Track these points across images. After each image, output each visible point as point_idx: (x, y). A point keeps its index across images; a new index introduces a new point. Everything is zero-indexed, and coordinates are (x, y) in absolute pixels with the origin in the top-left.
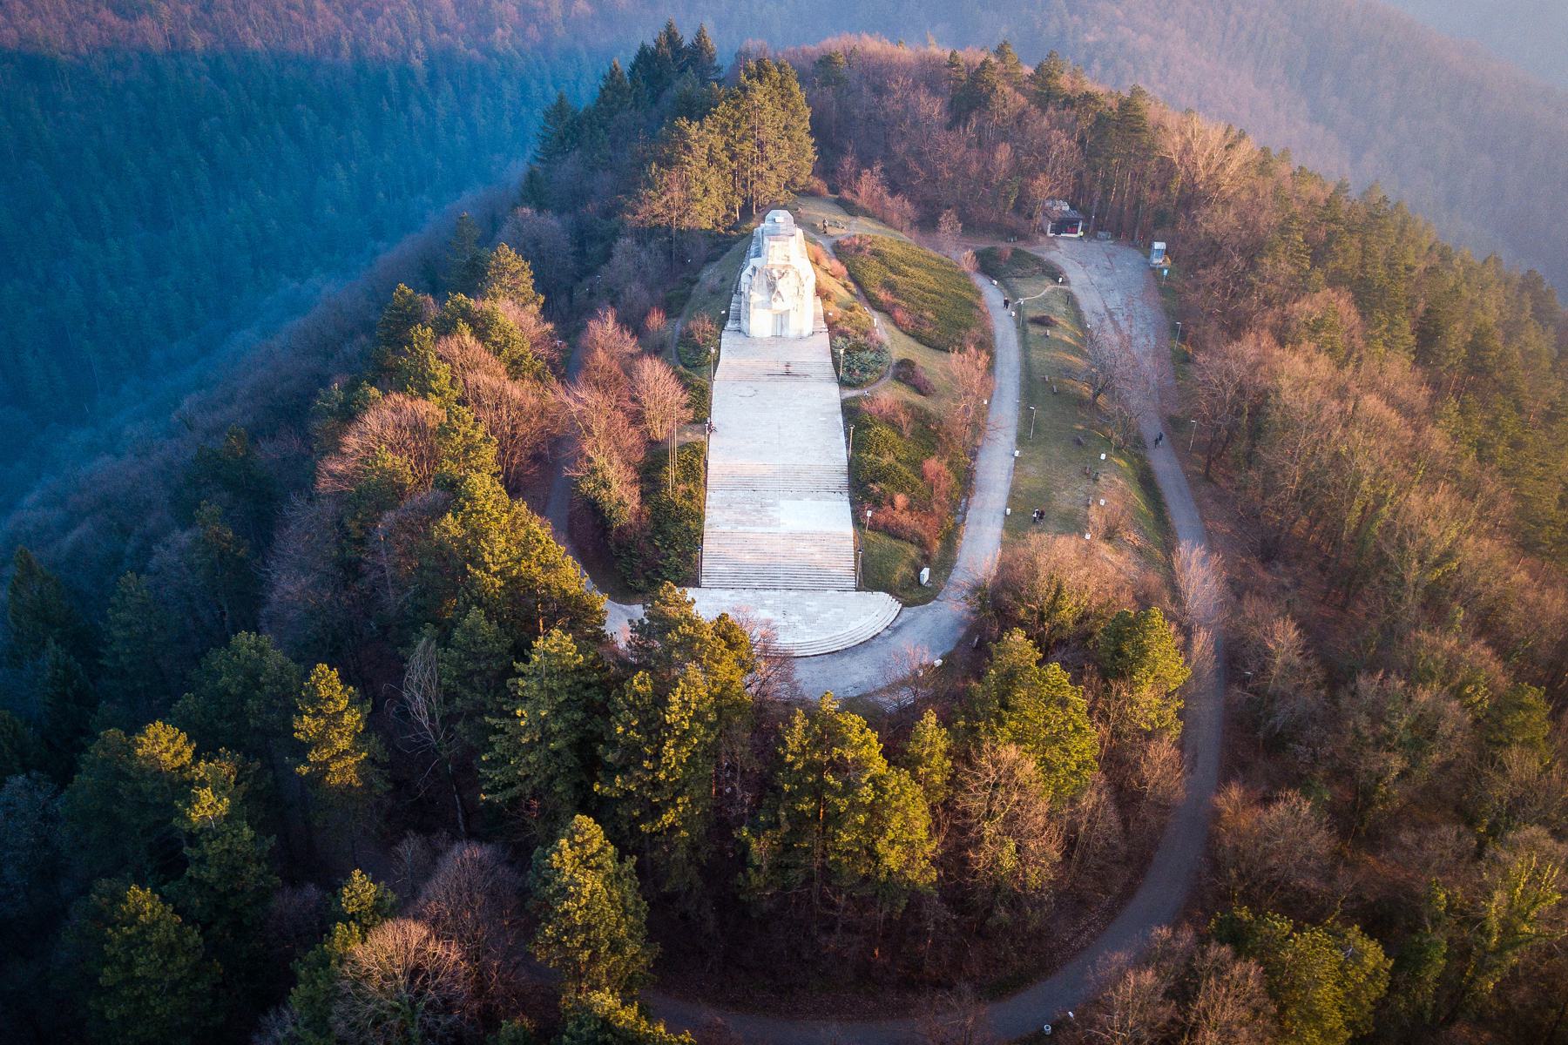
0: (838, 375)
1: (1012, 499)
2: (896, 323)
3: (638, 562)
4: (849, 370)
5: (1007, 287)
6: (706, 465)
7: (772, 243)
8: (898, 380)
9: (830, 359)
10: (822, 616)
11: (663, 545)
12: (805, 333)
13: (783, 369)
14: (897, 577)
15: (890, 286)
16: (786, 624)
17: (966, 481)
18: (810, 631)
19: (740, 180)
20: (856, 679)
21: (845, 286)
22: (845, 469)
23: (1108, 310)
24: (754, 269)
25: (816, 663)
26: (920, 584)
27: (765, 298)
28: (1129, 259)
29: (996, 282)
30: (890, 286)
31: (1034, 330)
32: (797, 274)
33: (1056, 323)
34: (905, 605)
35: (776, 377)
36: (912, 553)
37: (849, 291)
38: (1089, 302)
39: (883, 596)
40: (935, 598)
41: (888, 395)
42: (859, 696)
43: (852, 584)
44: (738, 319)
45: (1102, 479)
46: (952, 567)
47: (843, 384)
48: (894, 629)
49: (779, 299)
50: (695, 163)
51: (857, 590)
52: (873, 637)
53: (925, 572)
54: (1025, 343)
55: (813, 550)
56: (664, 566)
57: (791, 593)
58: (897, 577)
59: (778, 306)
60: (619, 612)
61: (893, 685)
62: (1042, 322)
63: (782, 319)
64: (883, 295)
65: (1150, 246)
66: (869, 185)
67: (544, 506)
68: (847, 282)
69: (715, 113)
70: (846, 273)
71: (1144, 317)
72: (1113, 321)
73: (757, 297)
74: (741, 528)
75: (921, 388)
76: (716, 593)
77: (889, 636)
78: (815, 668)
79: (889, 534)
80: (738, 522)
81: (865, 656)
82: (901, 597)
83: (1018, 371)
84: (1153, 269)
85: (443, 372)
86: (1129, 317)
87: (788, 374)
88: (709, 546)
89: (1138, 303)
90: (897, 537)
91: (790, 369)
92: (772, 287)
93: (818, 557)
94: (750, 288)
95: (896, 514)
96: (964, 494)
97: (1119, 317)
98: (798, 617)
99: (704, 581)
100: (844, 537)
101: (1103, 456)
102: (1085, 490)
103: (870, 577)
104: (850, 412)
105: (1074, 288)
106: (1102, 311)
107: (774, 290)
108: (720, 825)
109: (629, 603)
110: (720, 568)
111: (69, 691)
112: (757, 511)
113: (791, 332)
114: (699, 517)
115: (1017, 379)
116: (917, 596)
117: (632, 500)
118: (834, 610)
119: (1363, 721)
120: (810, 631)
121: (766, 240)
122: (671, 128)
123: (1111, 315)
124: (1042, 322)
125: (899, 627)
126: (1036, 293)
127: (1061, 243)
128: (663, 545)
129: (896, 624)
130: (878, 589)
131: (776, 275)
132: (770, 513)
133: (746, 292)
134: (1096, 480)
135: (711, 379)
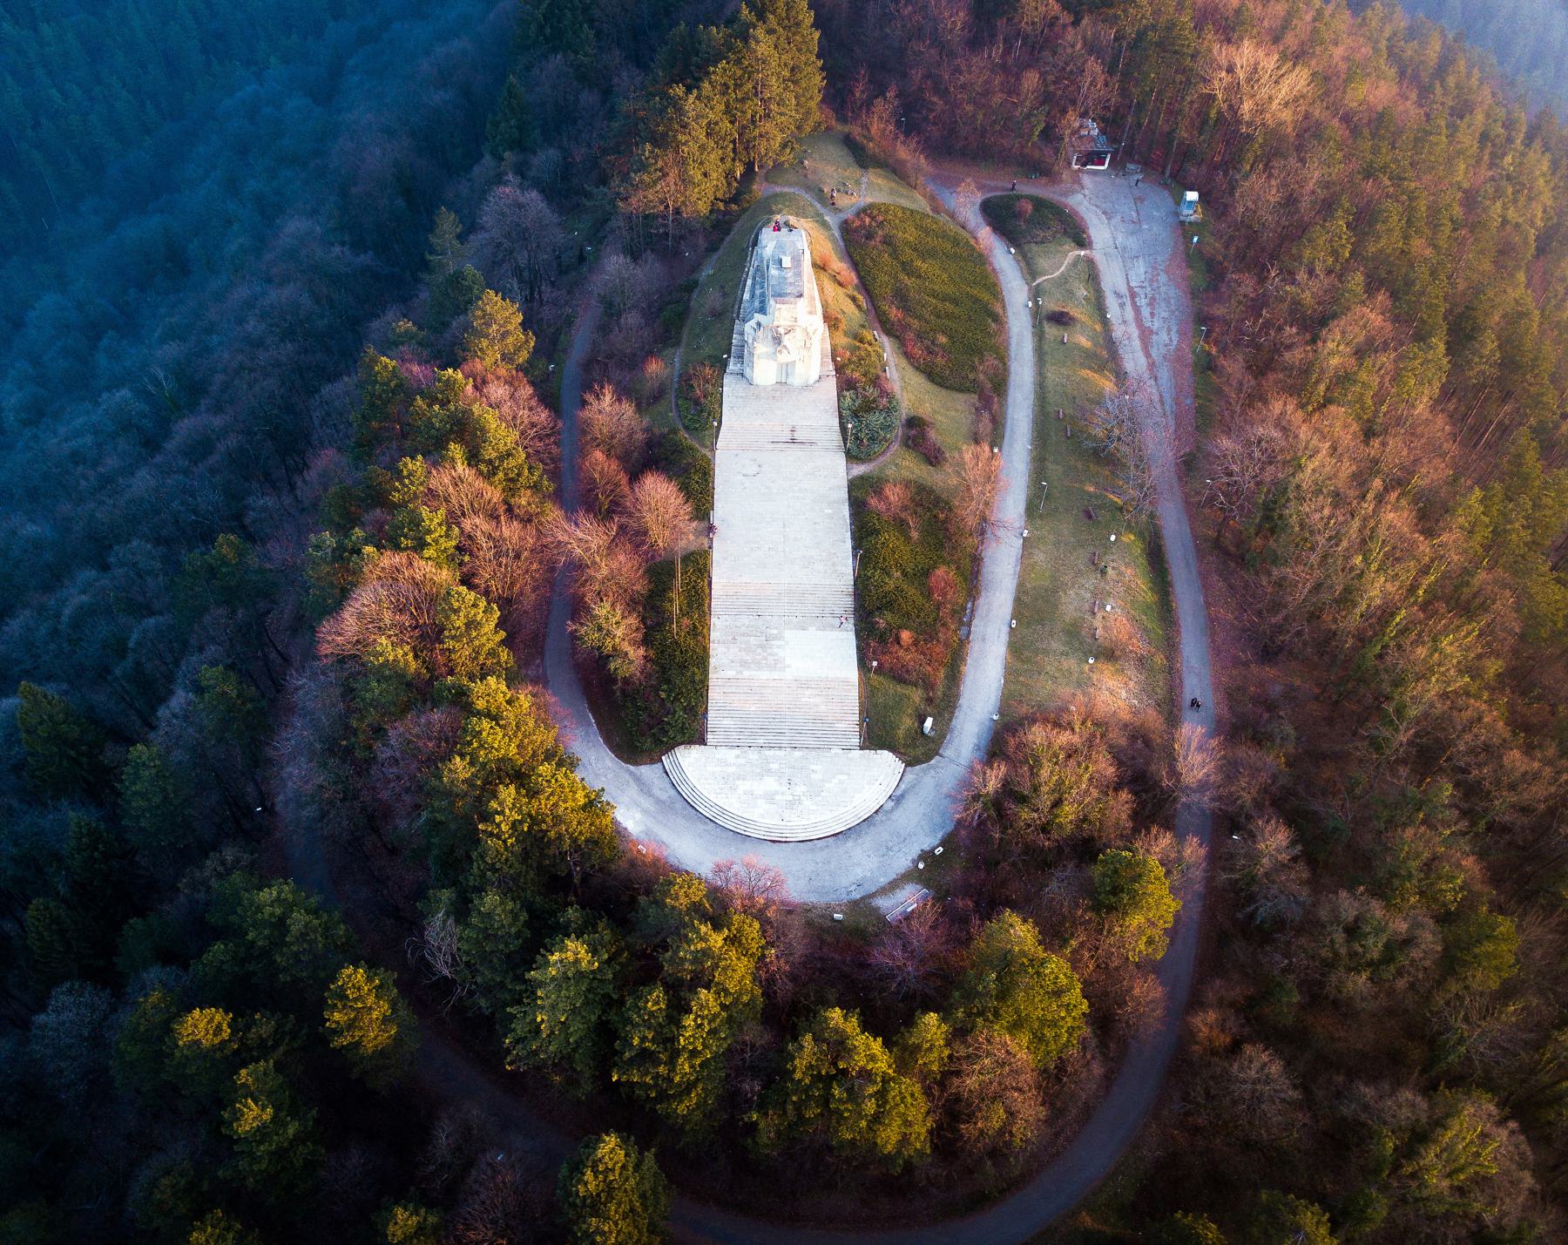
0: (845, 444)
1: (1018, 601)
2: (908, 355)
3: (643, 716)
4: (857, 438)
5: (1024, 257)
6: (710, 584)
7: (778, 306)
8: (908, 446)
9: (837, 420)
10: (827, 785)
11: (669, 696)
12: (811, 381)
13: (787, 436)
14: (901, 733)
15: (901, 297)
16: (791, 798)
17: (972, 577)
18: (814, 807)
19: (743, 145)
20: (859, 873)
21: (854, 299)
22: (851, 589)
23: (1130, 289)
24: (759, 324)
25: (822, 849)
26: (922, 732)
27: (771, 349)
28: (1157, 203)
29: (1013, 251)
30: (901, 297)
31: (1051, 331)
32: (805, 330)
33: (1072, 319)
34: (909, 764)
35: (780, 445)
36: (917, 700)
37: (859, 307)
38: (1112, 278)
39: (886, 755)
40: (937, 754)
41: (899, 465)
42: (862, 898)
43: (856, 741)
44: (741, 357)
45: (1109, 570)
46: (955, 708)
47: (851, 457)
48: (897, 799)
49: (785, 351)
50: (693, 140)
51: (862, 748)
52: (876, 812)
53: (929, 722)
54: (1039, 336)
55: (817, 700)
56: (669, 723)
57: (797, 753)
58: (901, 733)
59: (784, 358)
60: (627, 776)
61: (895, 881)
62: (1060, 319)
63: (787, 368)
64: (894, 313)
65: (1182, 196)
66: (878, 125)
67: (546, 616)
68: (856, 293)
69: (714, 72)
70: (856, 281)
71: (1167, 300)
72: (1134, 304)
73: (761, 349)
74: (746, 673)
75: (933, 457)
76: (723, 753)
77: (892, 810)
78: (820, 856)
79: (894, 677)
80: (744, 664)
81: (868, 840)
82: (904, 754)
83: (1032, 397)
84: (1182, 223)
85: (433, 519)
86: (1152, 302)
87: (793, 441)
88: (715, 695)
89: (1163, 278)
90: (901, 680)
91: (796, 435)
92: (777, 340)
93: (823, 708)
94: (754, 340)
95: (901, 653)
96: (970, 596)
97: (1142, 302)
98: (804, 789)
99: (709, 736)
100: (846, 682)
101: (1113, 538)
102: (1092, 588)
103: (876, 734)
104: (861, 496)
105: (1097, 256)
106: (1123, 290)
107: (779, 344)
108: (732, 1101)
109: (636, 763)
110: (726, 722)
111: (96, 854)
112: (761, 646)
113: (796, 380)
114: (702, 661)
115: (1030, 411)
116: (920, 751)
117: (636, 654)
118: (838, 777)
119: (1339, 937)
120: (814, 807)
121: (772, 302)
122: (665, 96)
123: (1133, 295)
124: (1060, 319)
125: (902, 796)
126: (1060, 261)
127: (1087, 180)
128: (669, 696)
129: (899, 793)
130: (882, 748)
131: (781, 330)
132: (775, 650)
133: (750, 341)
134: (1103, 572)
135: (713, 450)
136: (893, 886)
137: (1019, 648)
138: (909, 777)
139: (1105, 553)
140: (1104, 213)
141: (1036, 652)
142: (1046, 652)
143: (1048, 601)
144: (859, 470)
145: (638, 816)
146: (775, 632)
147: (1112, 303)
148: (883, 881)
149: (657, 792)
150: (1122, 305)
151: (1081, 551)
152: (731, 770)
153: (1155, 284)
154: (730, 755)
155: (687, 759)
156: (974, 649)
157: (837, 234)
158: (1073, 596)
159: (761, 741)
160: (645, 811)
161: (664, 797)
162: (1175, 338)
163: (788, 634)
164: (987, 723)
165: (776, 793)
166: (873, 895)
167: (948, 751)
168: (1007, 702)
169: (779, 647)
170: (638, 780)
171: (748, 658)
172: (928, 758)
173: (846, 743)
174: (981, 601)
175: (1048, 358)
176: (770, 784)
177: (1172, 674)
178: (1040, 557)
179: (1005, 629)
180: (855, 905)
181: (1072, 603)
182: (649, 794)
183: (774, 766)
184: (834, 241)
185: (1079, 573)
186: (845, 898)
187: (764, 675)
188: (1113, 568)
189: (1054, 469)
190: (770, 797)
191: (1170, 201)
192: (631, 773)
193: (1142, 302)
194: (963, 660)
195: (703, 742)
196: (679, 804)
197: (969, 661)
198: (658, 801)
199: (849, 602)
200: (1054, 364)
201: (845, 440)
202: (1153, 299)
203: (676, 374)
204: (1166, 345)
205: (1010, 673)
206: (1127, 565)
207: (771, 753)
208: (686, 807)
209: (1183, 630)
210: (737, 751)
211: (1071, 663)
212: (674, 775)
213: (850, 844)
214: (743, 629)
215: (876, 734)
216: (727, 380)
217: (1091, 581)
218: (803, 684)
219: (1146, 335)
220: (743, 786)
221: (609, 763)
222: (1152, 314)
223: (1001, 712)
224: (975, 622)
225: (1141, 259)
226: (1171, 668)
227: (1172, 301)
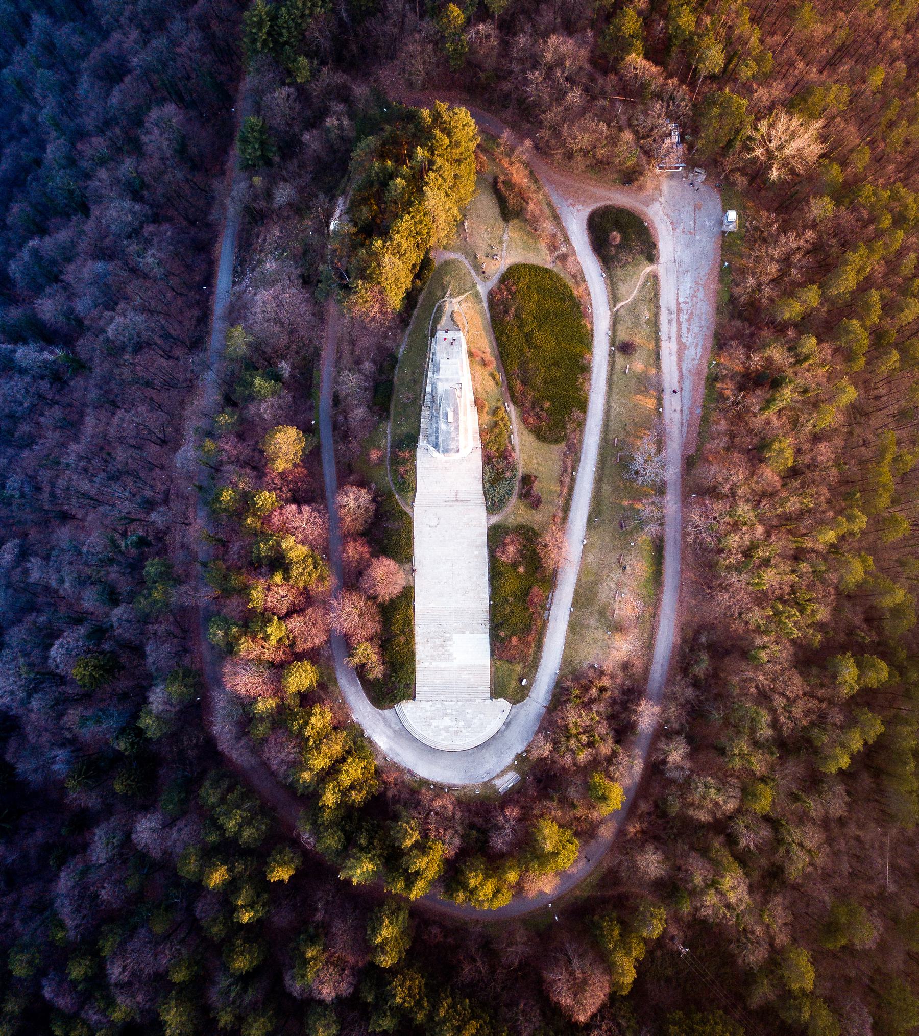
1: (576, 592)
13: (453, 498)
14: (510, 691)
23: (678, 303)
31: (620, 359)
34: (514, 703)
38: (667, 297)
43: (489, 695)
57: (460, 703)
68: (496, 373)
71: (700, 317)
74: (434, 664)
84: (724, 233)
97: (684, 317)
101: (632, 544)
103: (497, 691)
106: (674, 307)
109: (382, 709)
110: (426, 689)
112: (442, 646)
123: (679, 310)
134: (624, 568)
135: (412, 508)
136: (503, 773)
137: (575, 627)
138: (514, 710)
139: (627, 555)
140: (672, 223)
141: (581, 628)
142: (587, 627)
143: (591, 591)
144: (494, 519)
145: (385, 739)
146: (448, 635)
147: (664, 318)
148: (498, 771)
149: (393, 726)
150: (670, 321)
151: (614, 553)
152: (428, 714)
153: (695, 299)
154: (427, 705)
155: (406, 708)
156: (551, 626)
157: (485, 304)
158: (606, 587)
159: (442, 697)
160: (388, 737)
161: (397, 728)
162: (699, 353)
163: (456, 637)
164: (553, 675)
165: (450, 726)
166: (493, 779)
167: (533, 694)
168: (566, 662)
169: (450, 645)
170: (384, 718)
171: (435, 653)
172: (523, 699)
173: (484, 696)
174: (557, 593)
175: (614, 389)
176: (447, 721)
177: (652, 637)
178: (591, 558)
179: (568, 612)
180: (485, 784)
181: (604, 592)
182: (390, 727)
183: (449, 711)
184: (482, 313)
185: (611, 570)
186: (481, 781)
187: (443, 665)
188: (630, 565)
189: (607, 488)
190: (447, 729)
191: (720, 207)
192: (380, 715)
193: (684, 317)
194: (545, 635)
195: (414, 698)
196: (404, 733)
197: (548, 635)
198: (394, 731)
199: (486, 616)
200: (618, 394)
201: (486, 500)
202: (691, 314)
203: (389, 445)
204: (693, 360)
205: (568, 643)
206: (638, 561)
207: (446, 703)
208: (405, 734)
209: (665, 589)
210: (431, 703)
211: (599, 634)
212: (401, 716)
213: (484, 750)
214: (432, 635)
215: (497, 691)
216: (419, 453)
217: (616, 575)
218: (462, 669)
219: (682, 347)
220: (434, 723)
221: (369, 709)
222: (689, 330)
223: (561, 669)
224: (553, 607)
225: (690, 273)
226: (655, 614)
227: (704, 316)
